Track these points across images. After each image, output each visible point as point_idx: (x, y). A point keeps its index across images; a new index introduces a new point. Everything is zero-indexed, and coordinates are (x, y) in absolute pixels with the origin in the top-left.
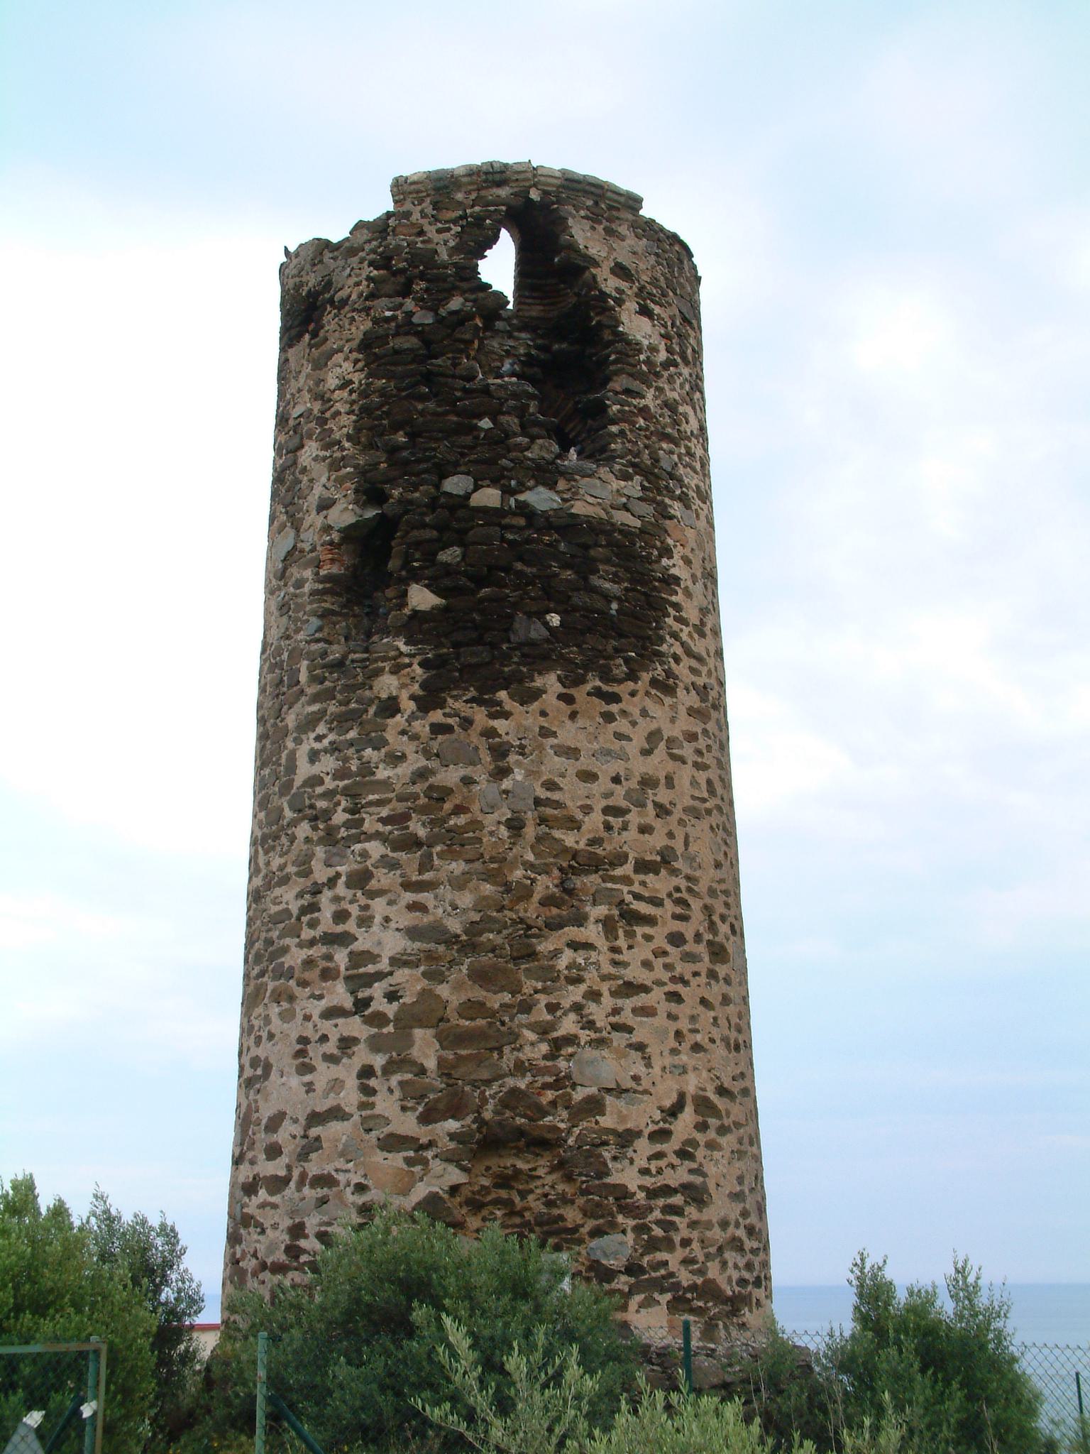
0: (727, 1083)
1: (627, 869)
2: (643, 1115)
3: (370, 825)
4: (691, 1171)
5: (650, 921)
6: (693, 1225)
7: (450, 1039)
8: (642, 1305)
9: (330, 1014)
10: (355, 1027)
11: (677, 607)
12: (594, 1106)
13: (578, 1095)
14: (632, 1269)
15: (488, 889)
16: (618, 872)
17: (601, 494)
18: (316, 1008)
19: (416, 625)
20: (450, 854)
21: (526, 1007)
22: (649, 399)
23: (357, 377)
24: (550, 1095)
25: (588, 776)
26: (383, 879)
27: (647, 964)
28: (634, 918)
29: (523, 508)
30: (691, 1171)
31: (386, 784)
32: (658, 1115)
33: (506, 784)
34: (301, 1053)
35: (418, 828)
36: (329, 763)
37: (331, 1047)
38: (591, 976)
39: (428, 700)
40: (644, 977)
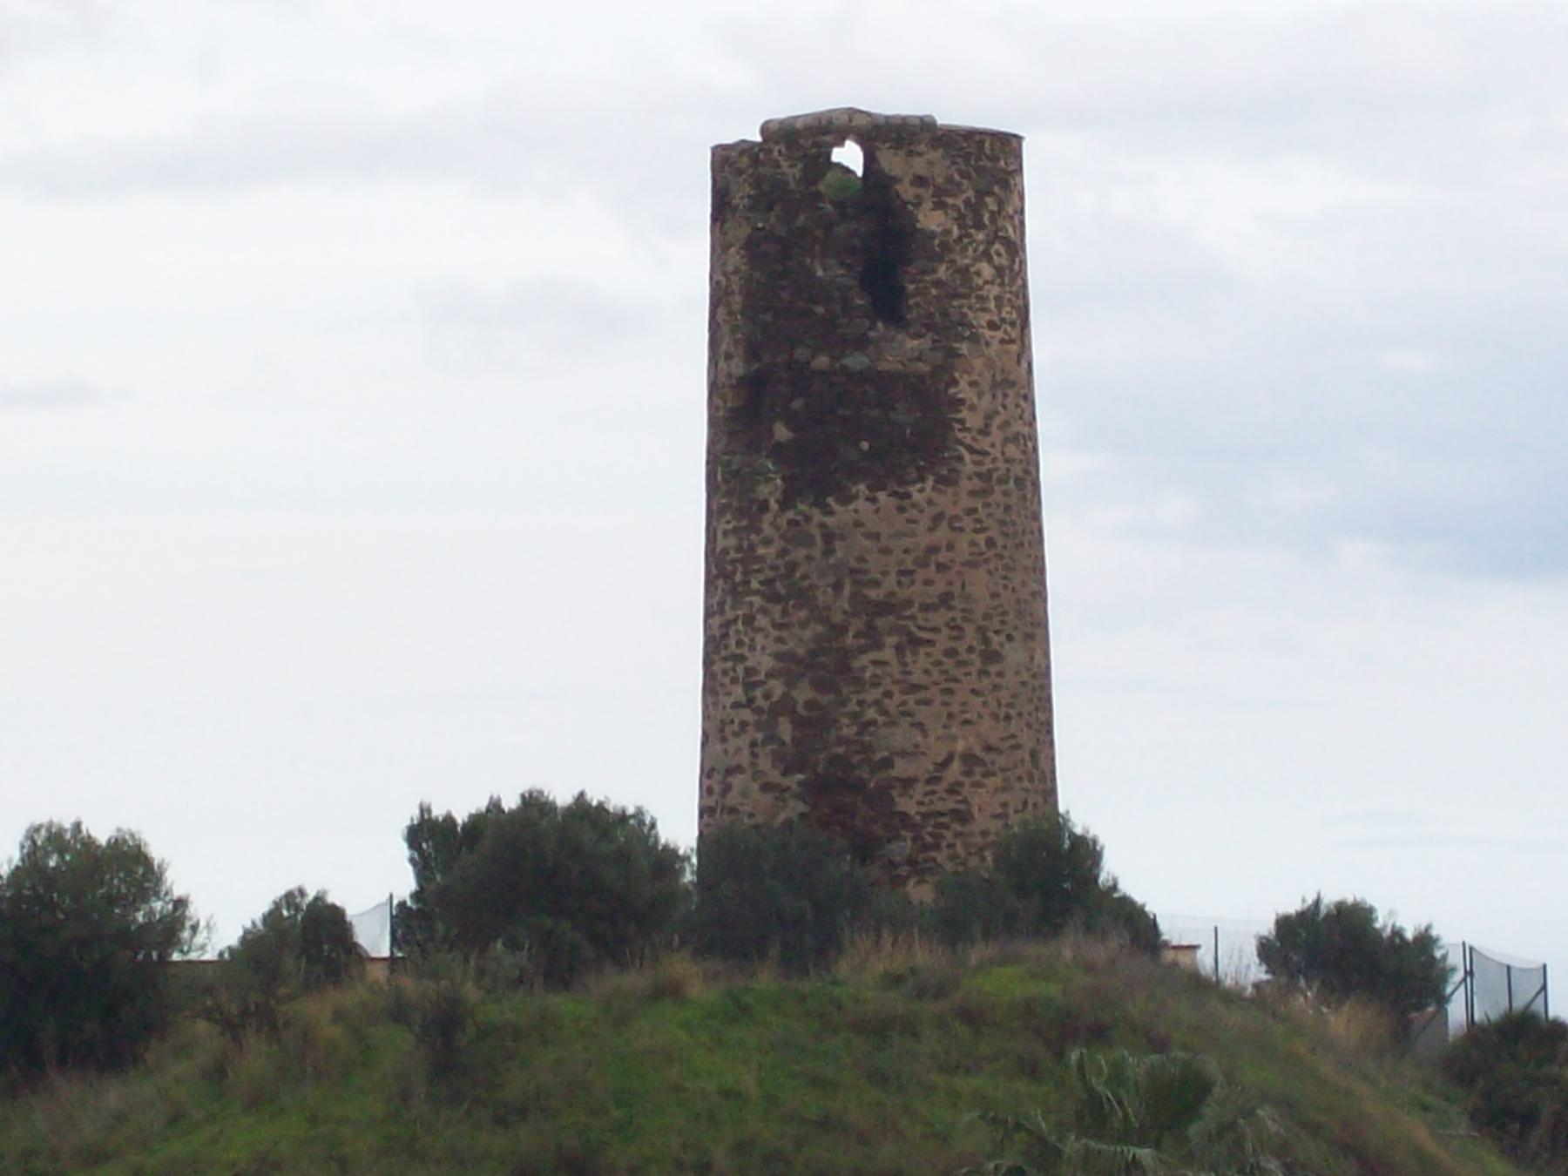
0: (993, 741)
1: (915, 609)
2: (919, 768)
3: (755, 585)
4: (958, 802)
5: (930, 642)
6: (958, 835)
7: (799, 723)
8: (918, 882)
9: (736, 705)
10: (747, 715)
11: (962, 422)
12: (887, 763)
13: (878, 756)
14: (911, 862)
16: (908, 613)
17: (904, 350)
18: (729, 701)
19: (778, 452)
20: (798, 607)
21: (844, 703)
22: (942, 272)
23: (743, 268)
24: (858, 758)
25: (886, 551)
26: (762, 621)
27: (926, 672)
28: (916, 642)
29: (844, 368)
30: (958, 802)
32: (932, 768)
34: (722, 730)
35: (780, 587)
36: (732, 541)
37: (736, 727)
38: (887, 683)
39: (786, 503)
40: (924, 680)
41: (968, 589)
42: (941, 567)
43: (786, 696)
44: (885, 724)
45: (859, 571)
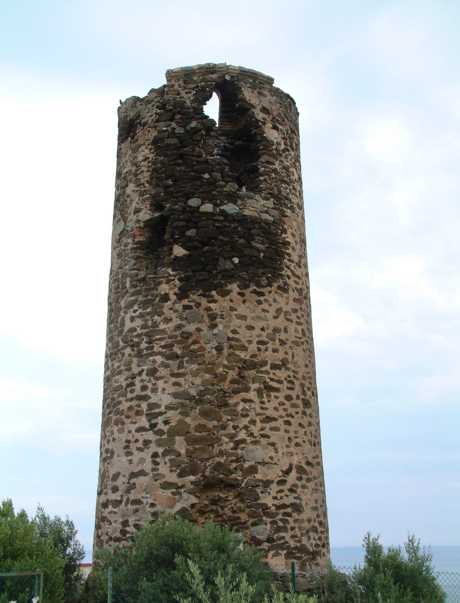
1: (268, 368)
2: (274, 474)
3: (156, 349)
4: (295, 498)
5: (277, 390)
6: (296, 521)
7: (191, 441)
10: (150, 435)
11: (289, 255)
12: (253, 470)
13: (246, 465)
15: (207, 376)
16: (264, 369)
17: (256, 206)
18: (133, 427)
19: (177, 263)
20: (191, 361)
21: (224, 427)
22: (277, 165)
24: (234, 465)
25: (251, 328)
26: (162, 372)
27: (276, 409)
28: (270, 389)
29: (223, 212)
30: (295, 498)
31: (164, 331)
32: (280, 474)
33: (215, 331)
35: (177, 350)
37: (140, 444)
38: (252, 414)
39: (182, 295)
40: (274, 414)
41: (296, 359)
42: (283, 343)
43: (180, 422)
44: (252, 442)
45: (233, 339)
